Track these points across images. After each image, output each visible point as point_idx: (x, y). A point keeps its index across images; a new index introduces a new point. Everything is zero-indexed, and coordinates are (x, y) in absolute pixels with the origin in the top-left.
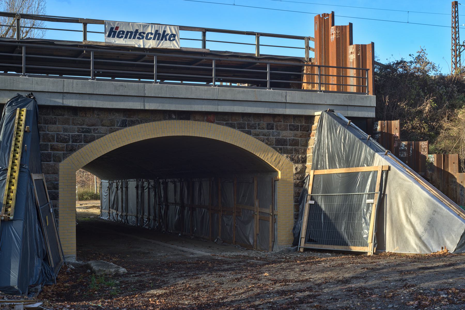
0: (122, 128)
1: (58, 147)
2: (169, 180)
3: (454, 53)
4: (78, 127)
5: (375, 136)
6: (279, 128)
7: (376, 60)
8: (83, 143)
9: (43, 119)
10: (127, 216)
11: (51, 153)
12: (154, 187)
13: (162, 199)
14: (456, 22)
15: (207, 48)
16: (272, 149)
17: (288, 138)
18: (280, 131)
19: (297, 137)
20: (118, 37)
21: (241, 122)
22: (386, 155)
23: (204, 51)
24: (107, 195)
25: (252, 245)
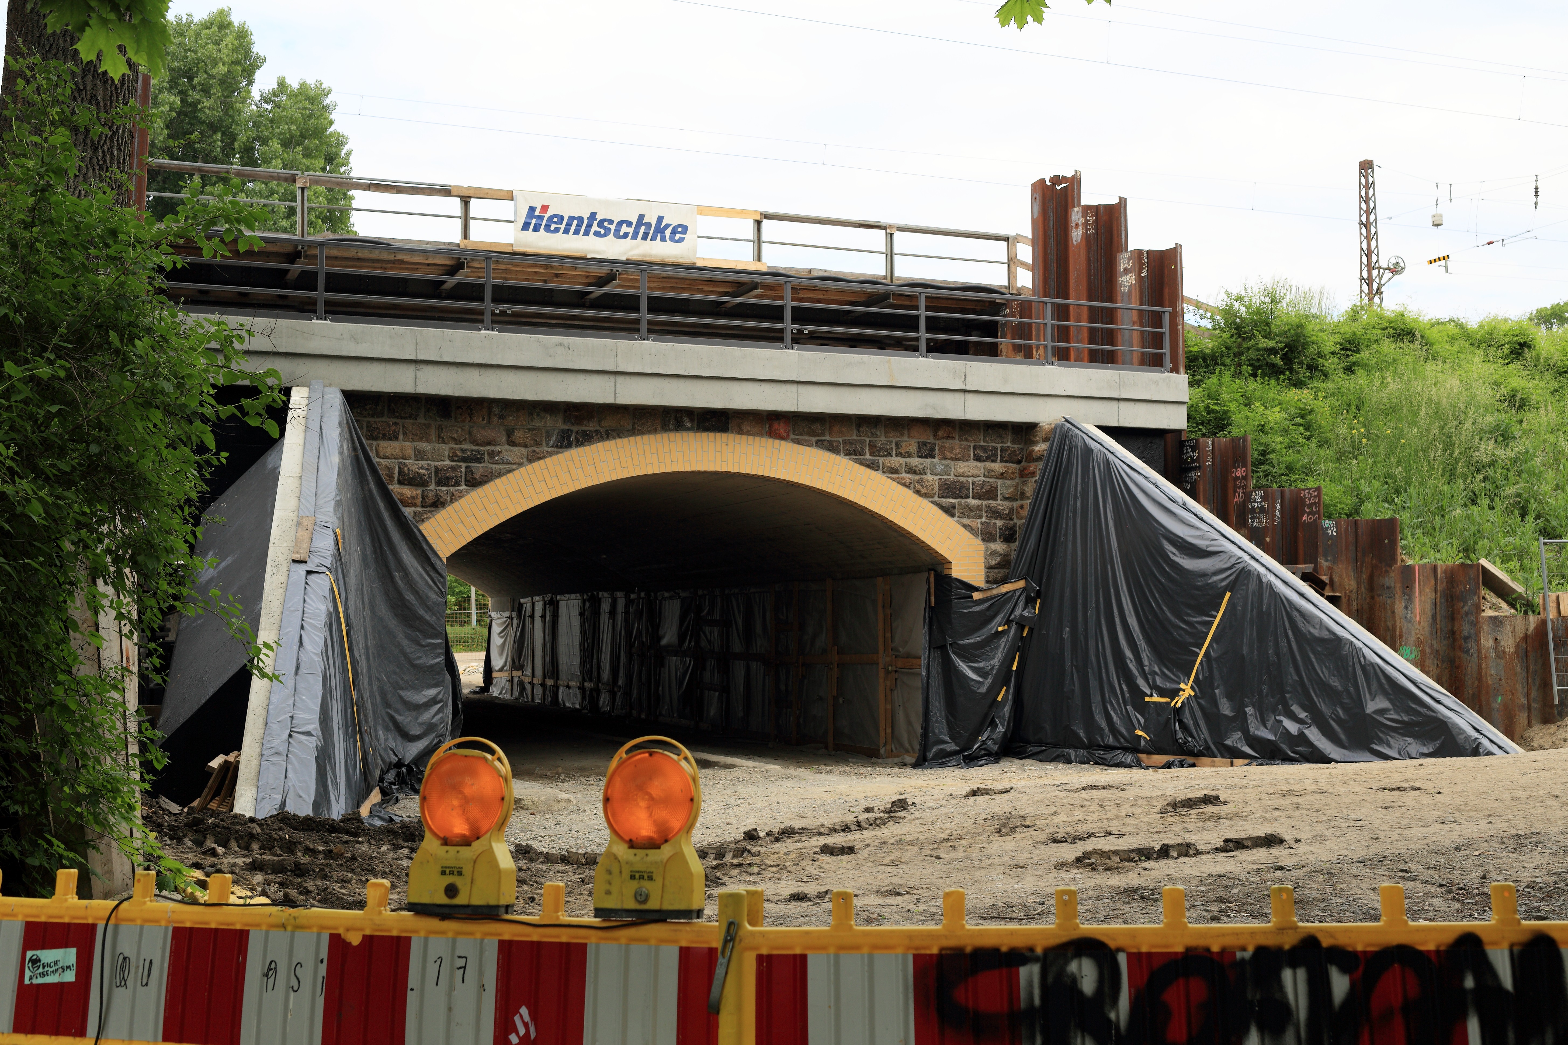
19: (992, 477)
20: (547, 228)
21: (855, 437)
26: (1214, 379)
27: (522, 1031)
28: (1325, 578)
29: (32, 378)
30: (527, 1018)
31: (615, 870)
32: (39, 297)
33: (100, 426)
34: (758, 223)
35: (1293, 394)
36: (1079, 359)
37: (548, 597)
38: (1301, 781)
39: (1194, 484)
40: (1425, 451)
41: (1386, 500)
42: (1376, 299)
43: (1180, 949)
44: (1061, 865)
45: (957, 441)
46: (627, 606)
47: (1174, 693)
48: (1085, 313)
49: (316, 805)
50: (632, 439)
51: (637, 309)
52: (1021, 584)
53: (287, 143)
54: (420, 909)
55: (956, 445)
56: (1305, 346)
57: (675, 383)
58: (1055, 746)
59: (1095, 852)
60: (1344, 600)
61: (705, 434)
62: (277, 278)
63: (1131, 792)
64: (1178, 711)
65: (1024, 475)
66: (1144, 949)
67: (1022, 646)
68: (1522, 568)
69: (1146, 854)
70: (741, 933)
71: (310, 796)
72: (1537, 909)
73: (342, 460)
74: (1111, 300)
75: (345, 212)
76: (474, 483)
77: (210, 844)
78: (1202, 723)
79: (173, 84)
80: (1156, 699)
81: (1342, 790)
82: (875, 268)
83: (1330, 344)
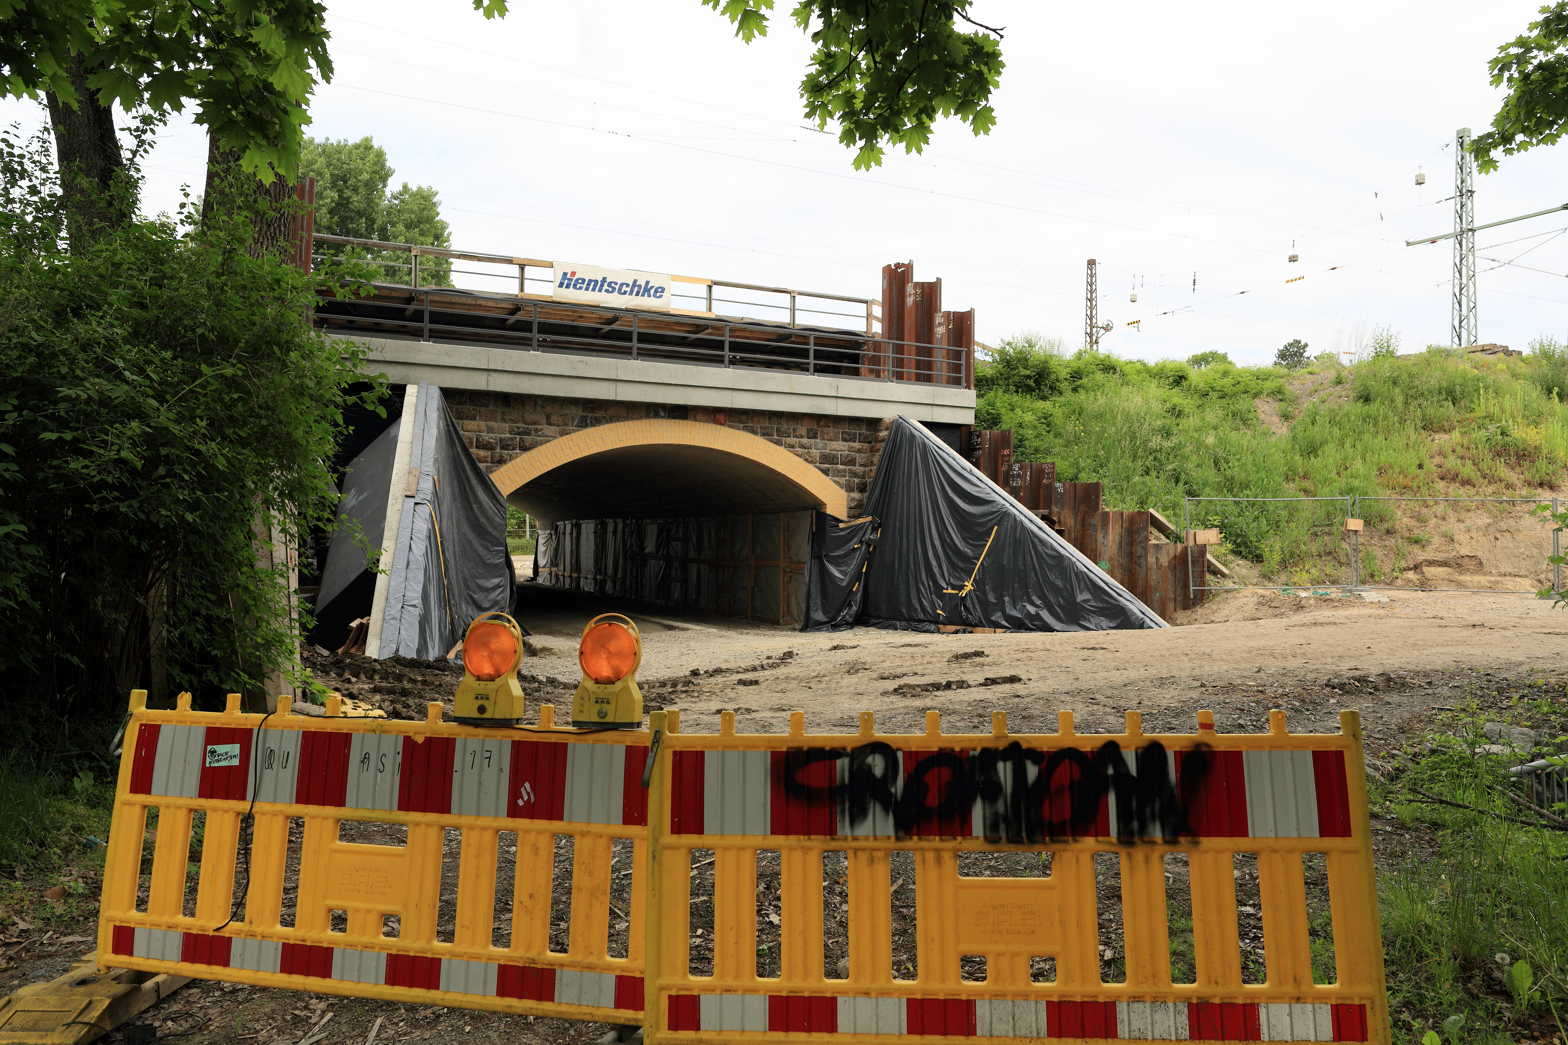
20: (575, 286)
26: (992, 394)
27: (526, 798)
28: (1055, 519)
29: (222, 376)
30: (529, 789)
31: (586, 698)
32: (226, 322)
33: (268, 408)
34: (710, 287)
35: (1040, 404)
36: (909, 379)
37: (574, 521)
38: (1035, 643)
39: (978, 459)
40: (1119, 441)
41: (1094, 471)
42: (1095, 347)
43: (935, 749)
44: (885, 693)
46: (624, 528)
47: (961, 588)
48: (914, 350)
49: (419, 651)
51: (630, 340)
52: (869, 519)
53: (409, 226)
54: (463, 721)
55: (831, 431)
56: (1049, 374)
57: (654, 387)
58: (887, 619)
59: (905, 685)
60: (1066, 532)
61: (673, 421)
62: (399, 314)
63: (931, 648)
64: (963, 599)
65: (873, 450)
66: (914, 749)
67: (869, 557)
68: (1175, 515)
69: (937, 687)
70: (663, 737)
71: (415, 646)
72: (1170, 723)
73: (439, 432)
74: (930, 342)
75: (448, 272)
76: (525, 448)
77: (347, 675)
78: (977, 606)
79: (334, 185)
80: (950, 591)
81: (1059, 649)
82: (782, 317)
83: (1064, 373)
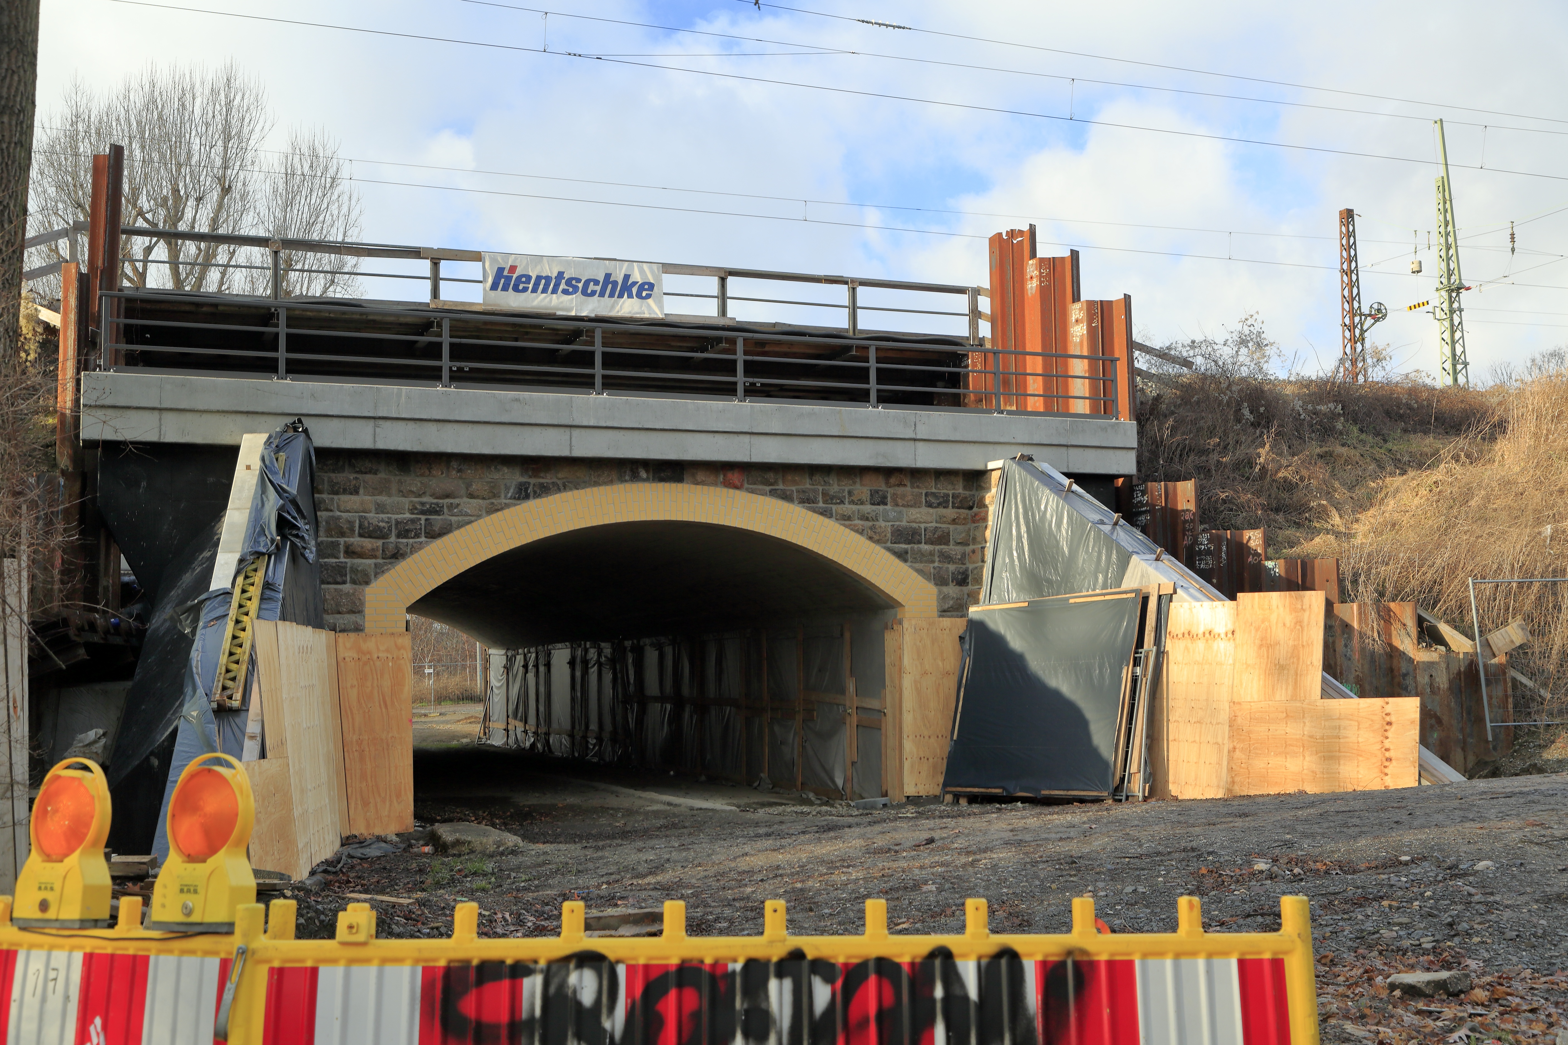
0: (518, 502)
1: (362, 547)
2: (647, 641)
3: (1347, 334)
4: (412, 502)
5: (1137, 520)
6: (900, 501)
7: (1137, 337)
8: (423, 539)
9: (326, 482)
10: (548, 734)
11: (346, 563)
12: (612, 661)
13: (632, 688)
14: (1352, 259)
15: (730, 314)
16: (883, 551)
17: (923, 526)
18: (902, 508)
19: (944, 523)
20: (516, 289)
21: (808, 486)
22: (1157, 559)
23: (722, 322)
24: (502, 685)
25: (841, 787)
45: (908, 489)
50: (588, 490)
55: (908, 490)
76: (434, 535)
82: (838, 320)
